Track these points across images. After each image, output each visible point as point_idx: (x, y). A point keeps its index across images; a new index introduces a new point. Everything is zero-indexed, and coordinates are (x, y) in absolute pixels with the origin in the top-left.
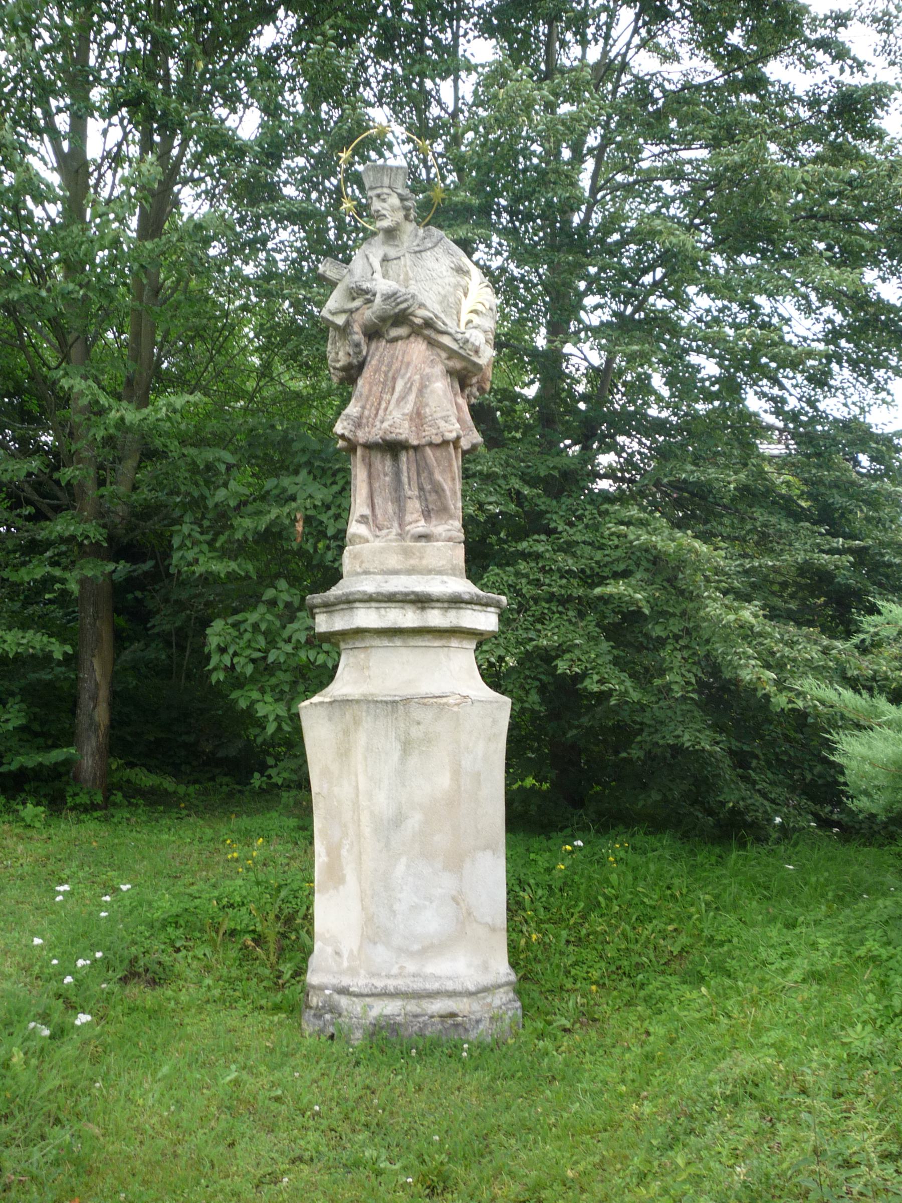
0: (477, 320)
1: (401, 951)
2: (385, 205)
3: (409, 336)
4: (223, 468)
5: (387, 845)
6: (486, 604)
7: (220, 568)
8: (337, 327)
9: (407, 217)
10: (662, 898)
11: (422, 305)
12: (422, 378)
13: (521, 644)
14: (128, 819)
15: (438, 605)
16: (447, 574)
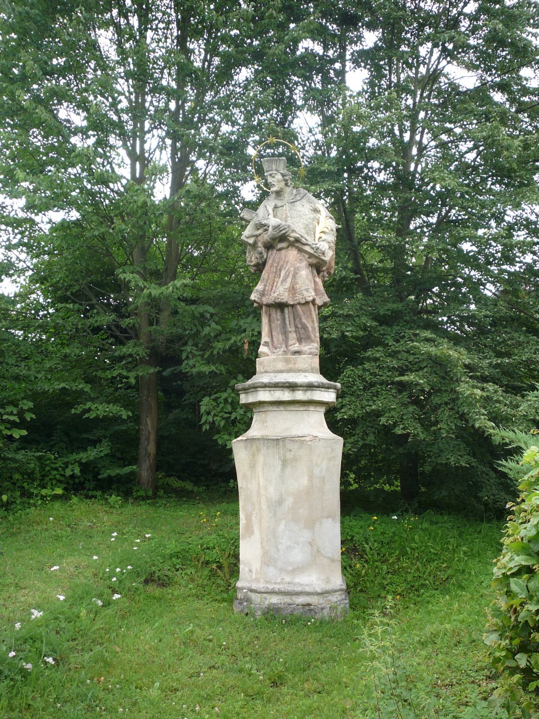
0: (324, 236)
1: (282, 570)
2: (274, 179)
3: (288, 247)
4: (208, 316)
5: (275, 514)
6: (328, 387)
7: (206, 369)
8: (250, 244)
9: (286, 185)
10: (442, 549)
11: (293, 231)
12: (295, 269)
13: (364, 408)
14: (165, 504)
15: (301, 388)
16: (308, 372)
